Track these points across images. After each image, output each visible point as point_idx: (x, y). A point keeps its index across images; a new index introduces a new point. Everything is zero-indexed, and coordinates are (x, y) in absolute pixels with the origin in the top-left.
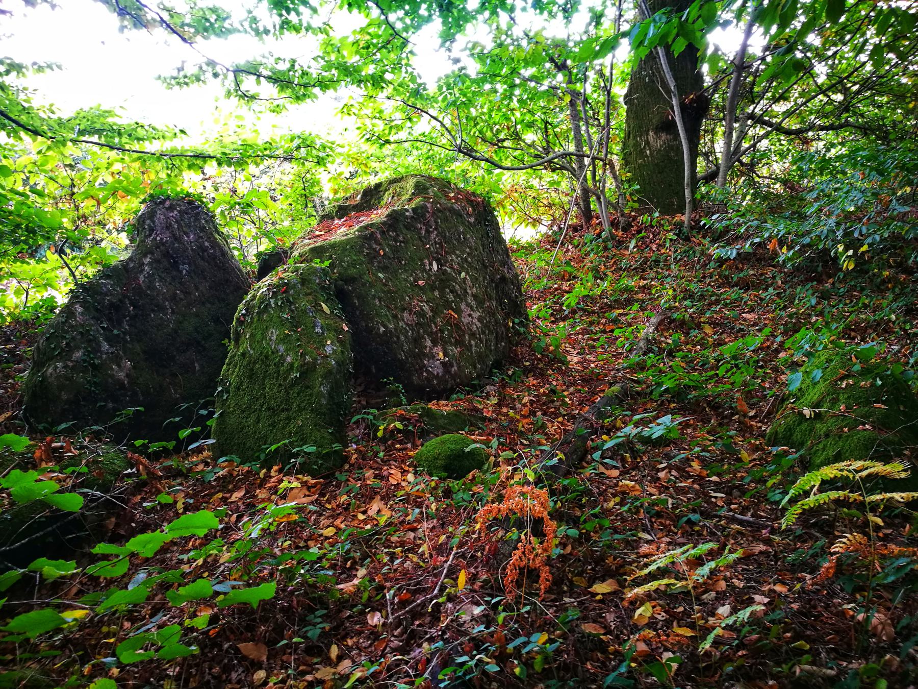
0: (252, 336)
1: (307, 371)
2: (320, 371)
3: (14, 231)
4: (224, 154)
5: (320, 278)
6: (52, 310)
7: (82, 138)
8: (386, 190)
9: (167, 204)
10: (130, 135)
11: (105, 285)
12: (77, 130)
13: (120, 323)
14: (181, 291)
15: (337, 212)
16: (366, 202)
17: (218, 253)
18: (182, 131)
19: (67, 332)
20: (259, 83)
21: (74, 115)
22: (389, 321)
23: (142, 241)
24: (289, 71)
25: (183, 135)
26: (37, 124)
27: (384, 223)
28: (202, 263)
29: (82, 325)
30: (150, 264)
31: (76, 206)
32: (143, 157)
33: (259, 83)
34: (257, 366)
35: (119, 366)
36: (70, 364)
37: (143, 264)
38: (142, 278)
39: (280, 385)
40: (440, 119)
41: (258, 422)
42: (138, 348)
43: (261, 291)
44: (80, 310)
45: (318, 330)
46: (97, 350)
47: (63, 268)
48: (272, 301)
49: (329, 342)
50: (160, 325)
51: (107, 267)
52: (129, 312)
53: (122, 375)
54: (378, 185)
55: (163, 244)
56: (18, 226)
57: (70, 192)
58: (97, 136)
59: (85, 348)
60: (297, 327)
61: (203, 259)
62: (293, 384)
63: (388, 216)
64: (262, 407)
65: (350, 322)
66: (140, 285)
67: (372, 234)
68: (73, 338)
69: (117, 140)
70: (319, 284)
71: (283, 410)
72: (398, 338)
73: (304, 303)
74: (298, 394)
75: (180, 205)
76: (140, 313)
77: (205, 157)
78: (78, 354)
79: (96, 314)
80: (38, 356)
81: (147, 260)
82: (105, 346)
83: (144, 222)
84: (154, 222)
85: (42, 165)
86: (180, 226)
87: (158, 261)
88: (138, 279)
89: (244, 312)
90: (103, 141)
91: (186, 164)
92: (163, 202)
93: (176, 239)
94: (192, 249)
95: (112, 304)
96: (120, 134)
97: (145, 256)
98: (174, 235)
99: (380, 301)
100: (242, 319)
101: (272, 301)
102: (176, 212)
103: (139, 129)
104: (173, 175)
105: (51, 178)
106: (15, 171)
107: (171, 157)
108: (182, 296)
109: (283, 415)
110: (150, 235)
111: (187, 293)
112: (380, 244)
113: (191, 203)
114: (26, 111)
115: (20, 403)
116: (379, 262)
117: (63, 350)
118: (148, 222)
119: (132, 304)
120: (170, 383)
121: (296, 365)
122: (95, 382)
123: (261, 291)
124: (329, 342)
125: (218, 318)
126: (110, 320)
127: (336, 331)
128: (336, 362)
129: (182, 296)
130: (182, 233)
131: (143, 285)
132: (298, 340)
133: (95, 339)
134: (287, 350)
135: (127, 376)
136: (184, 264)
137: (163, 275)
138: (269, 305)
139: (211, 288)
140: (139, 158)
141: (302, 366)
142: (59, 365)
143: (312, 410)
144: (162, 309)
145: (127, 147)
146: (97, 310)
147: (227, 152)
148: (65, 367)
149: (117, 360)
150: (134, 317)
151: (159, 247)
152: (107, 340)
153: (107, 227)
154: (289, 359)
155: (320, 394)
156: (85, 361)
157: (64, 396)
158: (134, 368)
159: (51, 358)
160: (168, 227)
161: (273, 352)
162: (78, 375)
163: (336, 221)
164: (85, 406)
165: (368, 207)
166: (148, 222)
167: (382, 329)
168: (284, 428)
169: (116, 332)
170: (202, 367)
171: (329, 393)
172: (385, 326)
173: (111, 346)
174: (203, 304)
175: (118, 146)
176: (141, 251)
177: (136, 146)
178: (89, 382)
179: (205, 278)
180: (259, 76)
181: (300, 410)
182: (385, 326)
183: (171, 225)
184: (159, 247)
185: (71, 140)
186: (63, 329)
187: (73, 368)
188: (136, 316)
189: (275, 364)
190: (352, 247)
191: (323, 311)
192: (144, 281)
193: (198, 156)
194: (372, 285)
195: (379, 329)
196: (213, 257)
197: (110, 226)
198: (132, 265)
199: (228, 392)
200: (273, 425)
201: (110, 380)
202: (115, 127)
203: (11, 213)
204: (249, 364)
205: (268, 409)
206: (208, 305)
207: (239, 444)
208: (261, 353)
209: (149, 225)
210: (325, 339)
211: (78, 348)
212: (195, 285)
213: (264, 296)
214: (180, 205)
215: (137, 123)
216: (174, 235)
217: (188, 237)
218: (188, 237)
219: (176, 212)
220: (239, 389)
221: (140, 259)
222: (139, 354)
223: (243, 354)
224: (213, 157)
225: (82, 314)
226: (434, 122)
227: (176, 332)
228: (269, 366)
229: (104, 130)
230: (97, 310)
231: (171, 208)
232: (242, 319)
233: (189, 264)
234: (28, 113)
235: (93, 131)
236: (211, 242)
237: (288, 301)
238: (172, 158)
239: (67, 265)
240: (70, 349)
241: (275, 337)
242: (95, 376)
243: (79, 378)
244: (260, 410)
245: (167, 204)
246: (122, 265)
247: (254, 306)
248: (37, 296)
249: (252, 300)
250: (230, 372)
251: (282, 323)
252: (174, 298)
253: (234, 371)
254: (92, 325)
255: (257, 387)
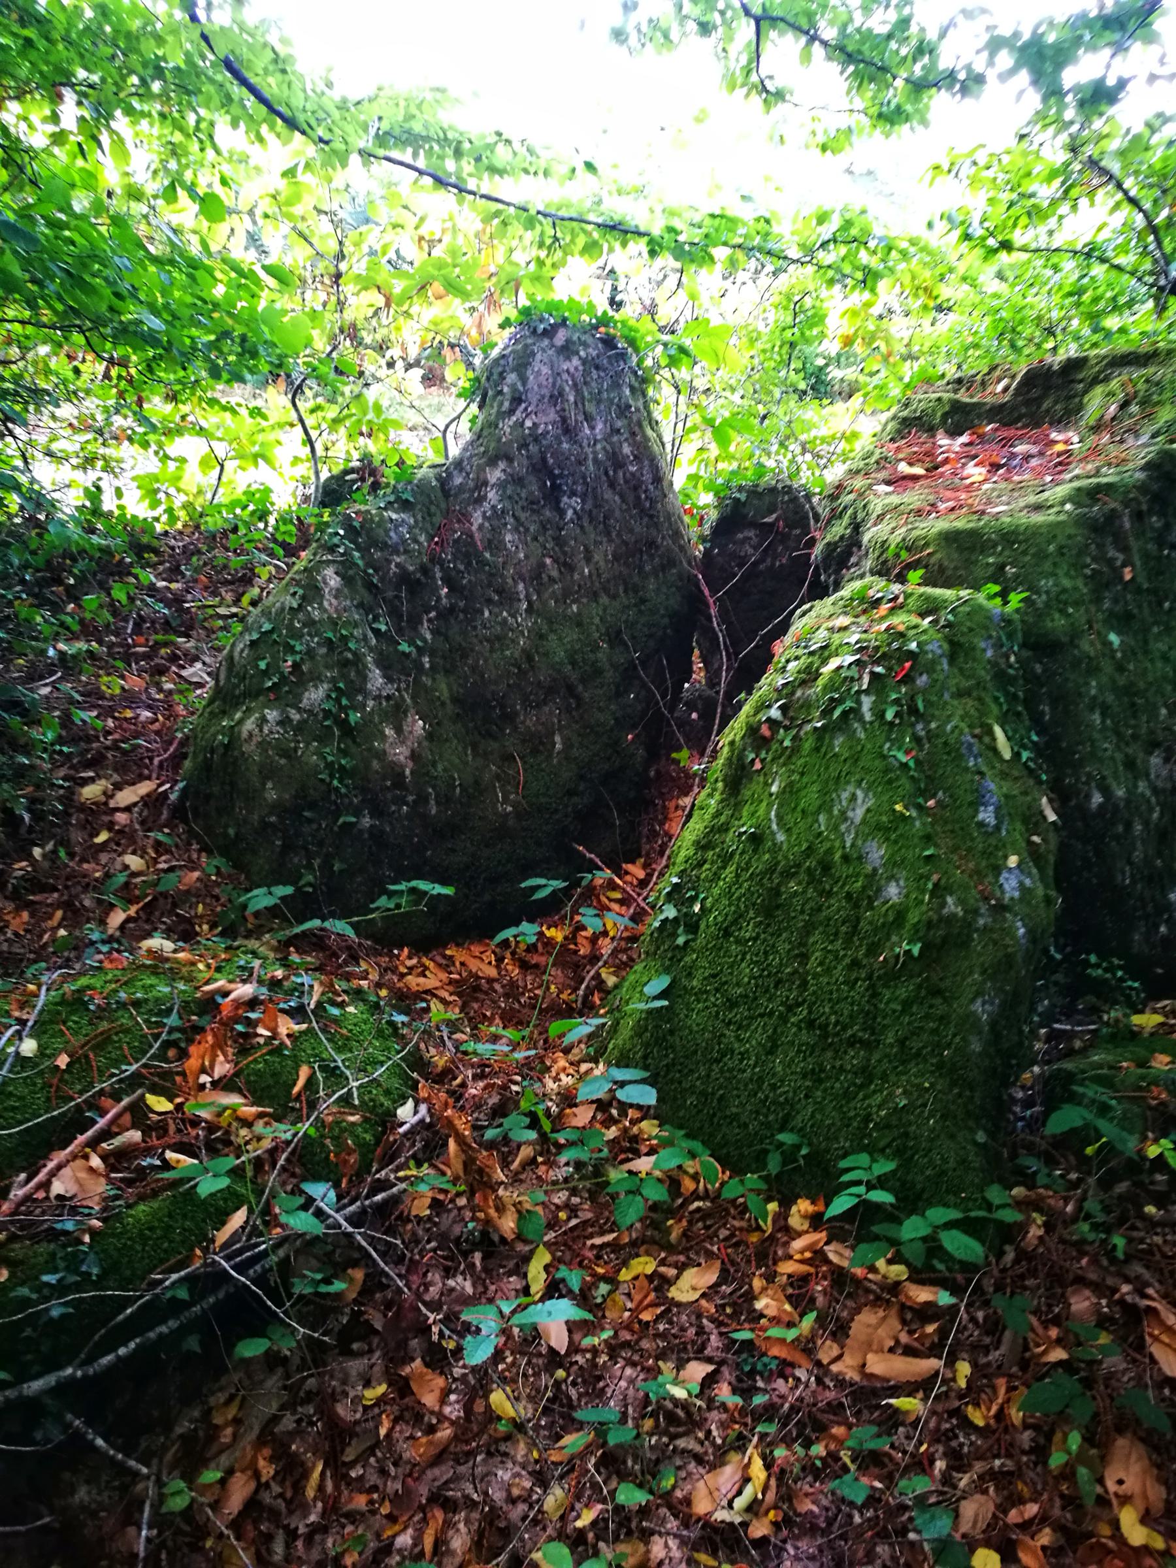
0: (790, 790)
1: (944, 941)
2: (981, 952)
3: (214, 346)
4: (671, 230)
5: (999, 645)
6: (263, 516)
7: (381, 152)
8: (1095, 381)
9: (561, 337)
10: (478, 159)
11: (397, 525)
12: (372, 132)
13: (415, 622)
14: (555, 561)
15: (945, 416)
16: (1027, 403)
17: (647, 477)
18: (589, 166)
19: (298, 636)
20: (806, 57)
21: (372, 92)
22: (1116, 777)
23: (491, 425)
24: (890, 36)
25: (589, 176)
26: (298, 101)
27: (1142, 488)
28: (608, 495)
29: (334, 623)
30: (501, 485)
31: (339, 302)
32: (502, 215)
33: (806, 57)
34: (793, 886)
35: (399, 730)
36: (295, 716)
37: (485, 483)
38: (477, 518)
39: (855, 964)
40: (1147, 206)
41: (771, 1052)
42: (443, 688)
43: (834, 663)
44: (334, 581)
45: (987, 815)
46: (355, 688)
47: (292, 425)
48: (867, 702)
49: (1013, 861)
50: (499, 638)
51: (923, 1215)
52: (439, 599)
53: (400, 753)
54: (1074, 365)
55: (536, 439)
56: (226, 334)
57: (332, 270)
58: (410, 150)
59: (333, 680)
60: (927, 794)
61: (612, 485)
62: (896, 972)
63: (1147, 467)
64: (790, 1009)
65: (1062, 797)
66: (471, 536)
67: (1112, 516)
68: (310, 653)
69: (450, 165)
70: (993, 663)
71: (852, 1042)
72: (1128, 826)
73: (954, 721)
74: (907, 1004)
75: (585, 345)
76: (462, 604)
77: (626, 232)
78: (315, 695)
79: (367, 598)
80: (228, 678)
81: (495, 475)
82: (376, 679)
83: (502, 375)
84: (524, 380)
85: (289, 203)
86: (580, 399)
87: (518, 481)
88: (465, 517)
89: (775, 713)
90: (421, 163)
91: (581, 240)
92: (550, 332)
93: (568, 430)
94: (595, 460)
95: (404, 577)
96: (458, 153)
97: (492, 462)
98: (564, 420)
99: (1104, 715)
100: (765, 731)
101: (867, 702)
102: (575, 361)
103: (500, 145)
104: (549, 262)
105: (301, 235)
106: (231, 212)
107: (556, 220)
108: (555, 574)
109: (854, 1058)
110: (512, 412)
111: (567, 567)
112: (1125, 549)
113: (609, 342)
114: (280, 64)
115: (177, 759)
116: (1115, 601)
117: (283, 678)
118: (512, 377)
119: (448, 581)
120: (498, 777)
121: (913, 917)
122: (342, 767)
123: (834, 663)
124: (1013, 861)
125: (619, 632)
126: (394, 613)
127: (1026, 821)
128: (1030, 931)
129: (555, 574)
130: (581, 418)
131: (477, 536)
132: (928, 839)
133: (358, 658)
134: (893, 863)
135: (414, 756)
136: (573, 494)
137: (523, 516)
138: (856, 712)
139: (616, 558)
140: (497, 214)
141: (930, 924)
142: (272, 715)
143: (940, 1066)
144: (508, 598)
145: (471, 185)
146: (370, 586)
147: (678, 224)
148: (284, 722)
149: (396, 713)
150: (446, 614)
151: (525, 445)
152: (385, 664)
153: (388, 354)
154: (893, 891)
155: (970, 1020)
156: (327, 714)
157: (272, 795)
158: (430, 736)
159: (255, 693)
160: (556, 397)
161: (846, 858)
162: (308, 744)
163: (943, 441)
164: (309, 821)
165: (1031, 415)
166: (512, 377)
167: (1097, 799)
168: (848, 1096)
169: (404, 647)
170: (567, 742)
171: (993, 1024)
172: (1106, 791)
173: (389, 679)
174: (595, 596)
175: (453, 180)
176: (488, 446)
177: (487, 185)
178: (329, 765)
179: (608, 534)
180: (813, 39)
181: (905, 1055)
182: (1106, 791)
183: (561, 394)
184: (525, 445)
185: (361, 152)
186: (290, 627)
187: (300, 728)
188: (452, 610)
189: (849, 896)
190: (1061, 551)
191: (995, 750)
192: (481, 527)
193: (613, 228)
194: (1093, 670)
195: (1088, 797)
196: (635, 485)
197: (395, 352)
198: (458, 480)
199: (693, 927)
200: (817, 1076)
201: (375, 764)
202: (450, 135)
203: (216, 306)
204: (771, 870)
205: (811, 1024)
206: (604, 600)
207: (703, 1093)
208: (810, 851)
209: (513, 387)
210: (1003, 849)
211: (317, 679)
212: (587, 550)
213: (840, 681)
214: (585, 345)
215: (499, 134)
216: (564, 420)
217: (592, 428)
218: (592, 428)
219: (575, 361)
220: (727, 933)
221: (481, 469)
222: (443, 704)
223: (756, 839)
224: (640, 234)
225: (338, 594)
226: (1127, 208)
227: (530, 659)
228: (829, 894)
229: (427, 139)
230: (370, 586)
231: (567, 350)
232: (765, 731)
233: (584, 497)
234: (284, 71)
235: (411, 139)
236: (635, 445)
237: (913, 710)
238: (559, 229)
239: (301, 421)
240: (300, 678)
241: (858, 814)
242: (344, 753)
243: (311, 754)
244: (784, 1019)
245: (561, 337)
246: (439, 478)
247: (807, 705)
248: (241, 479)
249: (803, 683)
250: (705, 872)
251: (886, 778)
252: (536, 577)
253: (716, 877)
254: (356, 626)
255: (783, 947)
